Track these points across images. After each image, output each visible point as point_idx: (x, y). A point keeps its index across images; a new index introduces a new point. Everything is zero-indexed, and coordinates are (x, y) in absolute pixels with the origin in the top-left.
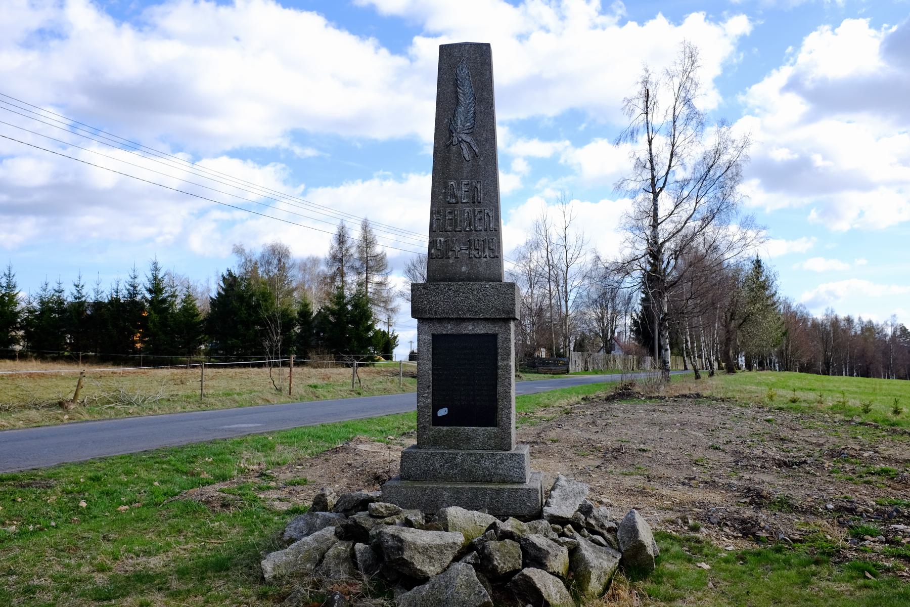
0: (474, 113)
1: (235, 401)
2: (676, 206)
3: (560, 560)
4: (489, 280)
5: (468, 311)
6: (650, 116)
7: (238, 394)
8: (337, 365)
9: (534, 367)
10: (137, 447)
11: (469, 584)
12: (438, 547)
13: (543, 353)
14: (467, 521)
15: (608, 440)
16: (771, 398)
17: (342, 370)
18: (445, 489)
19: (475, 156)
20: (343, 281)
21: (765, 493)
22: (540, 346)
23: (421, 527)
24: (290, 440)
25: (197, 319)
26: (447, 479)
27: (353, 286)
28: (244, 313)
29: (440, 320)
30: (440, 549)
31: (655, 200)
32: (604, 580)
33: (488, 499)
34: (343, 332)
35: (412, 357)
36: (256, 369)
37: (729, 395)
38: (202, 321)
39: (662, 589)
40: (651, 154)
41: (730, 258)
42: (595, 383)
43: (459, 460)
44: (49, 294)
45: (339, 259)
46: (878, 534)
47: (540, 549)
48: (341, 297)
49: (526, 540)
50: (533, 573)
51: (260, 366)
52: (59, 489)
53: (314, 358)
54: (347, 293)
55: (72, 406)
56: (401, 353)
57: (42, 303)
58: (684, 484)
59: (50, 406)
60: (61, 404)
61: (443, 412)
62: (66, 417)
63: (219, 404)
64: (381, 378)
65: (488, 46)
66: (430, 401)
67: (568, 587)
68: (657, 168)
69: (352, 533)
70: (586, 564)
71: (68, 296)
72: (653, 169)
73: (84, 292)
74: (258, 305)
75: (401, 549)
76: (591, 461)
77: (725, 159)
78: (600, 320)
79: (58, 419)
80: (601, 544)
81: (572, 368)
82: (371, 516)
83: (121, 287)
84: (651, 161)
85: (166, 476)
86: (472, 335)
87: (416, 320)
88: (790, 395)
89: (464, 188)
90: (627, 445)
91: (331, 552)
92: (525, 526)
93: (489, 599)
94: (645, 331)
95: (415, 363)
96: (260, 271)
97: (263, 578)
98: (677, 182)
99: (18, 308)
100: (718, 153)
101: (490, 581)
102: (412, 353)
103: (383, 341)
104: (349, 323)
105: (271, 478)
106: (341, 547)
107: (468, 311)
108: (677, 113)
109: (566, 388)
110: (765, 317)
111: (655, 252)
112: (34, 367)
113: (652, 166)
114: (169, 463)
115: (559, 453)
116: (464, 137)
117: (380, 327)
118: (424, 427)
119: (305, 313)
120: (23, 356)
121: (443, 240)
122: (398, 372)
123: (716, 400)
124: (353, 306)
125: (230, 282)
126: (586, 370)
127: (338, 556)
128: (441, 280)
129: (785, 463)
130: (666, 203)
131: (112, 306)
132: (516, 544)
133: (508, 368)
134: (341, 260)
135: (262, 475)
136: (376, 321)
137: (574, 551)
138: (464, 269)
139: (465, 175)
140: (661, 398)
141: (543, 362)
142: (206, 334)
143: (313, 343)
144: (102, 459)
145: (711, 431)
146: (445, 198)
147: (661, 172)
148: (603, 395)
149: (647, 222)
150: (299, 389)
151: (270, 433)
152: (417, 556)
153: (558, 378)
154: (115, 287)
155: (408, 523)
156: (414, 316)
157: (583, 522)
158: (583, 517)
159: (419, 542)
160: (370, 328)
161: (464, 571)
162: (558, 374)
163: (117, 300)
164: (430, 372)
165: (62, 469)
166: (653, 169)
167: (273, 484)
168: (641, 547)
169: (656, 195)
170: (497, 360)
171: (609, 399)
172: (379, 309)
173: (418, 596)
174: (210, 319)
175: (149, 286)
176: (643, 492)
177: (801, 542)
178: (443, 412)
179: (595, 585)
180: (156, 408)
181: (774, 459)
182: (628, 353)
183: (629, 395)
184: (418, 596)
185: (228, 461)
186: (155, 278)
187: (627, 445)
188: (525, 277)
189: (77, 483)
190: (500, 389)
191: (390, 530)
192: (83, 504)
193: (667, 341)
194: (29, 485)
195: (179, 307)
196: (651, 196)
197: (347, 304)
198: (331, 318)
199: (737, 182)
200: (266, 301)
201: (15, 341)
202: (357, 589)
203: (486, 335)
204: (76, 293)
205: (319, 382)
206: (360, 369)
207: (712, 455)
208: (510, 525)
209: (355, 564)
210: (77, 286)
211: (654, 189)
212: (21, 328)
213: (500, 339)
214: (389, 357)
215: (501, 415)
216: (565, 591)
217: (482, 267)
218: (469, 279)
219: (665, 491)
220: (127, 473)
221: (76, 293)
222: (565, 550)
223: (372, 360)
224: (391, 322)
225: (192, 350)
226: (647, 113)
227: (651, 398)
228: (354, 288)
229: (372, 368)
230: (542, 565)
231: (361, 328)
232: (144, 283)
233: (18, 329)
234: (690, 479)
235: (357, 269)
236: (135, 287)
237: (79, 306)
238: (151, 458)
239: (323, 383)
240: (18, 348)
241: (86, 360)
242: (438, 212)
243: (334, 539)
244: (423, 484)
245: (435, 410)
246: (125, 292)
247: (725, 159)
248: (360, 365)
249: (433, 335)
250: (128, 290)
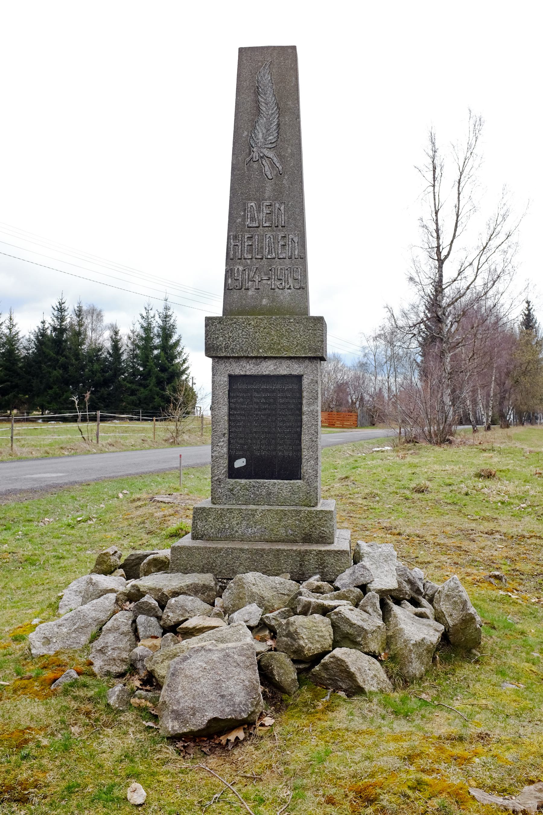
0: (278, 125)
5: (270, 348)
31: (440, 267)
34: (133, 383)
65: (294, 48)
66: (225, 450)
72: (438, 238)
86: (274, 376)
87: (210, 360)
107: (270, 348)
116: (266, 152)
121: (241, 268)
128: (240, 314)
138: (264, 302)
139: (266, 196)
147: (445, 241)
156: (208, 354)
164: (226, 418)
166: (438, 238)
169: (441, 262)
170: (301, 404)
178: (240, 463)
190: (305, 438)
203: (290, 376)
213: (305, 381)
215: (306, 467)
226: (434, 186)
239: (123, 446)
242: (235, 237)
245: (232, 459)
249: (230, 376)
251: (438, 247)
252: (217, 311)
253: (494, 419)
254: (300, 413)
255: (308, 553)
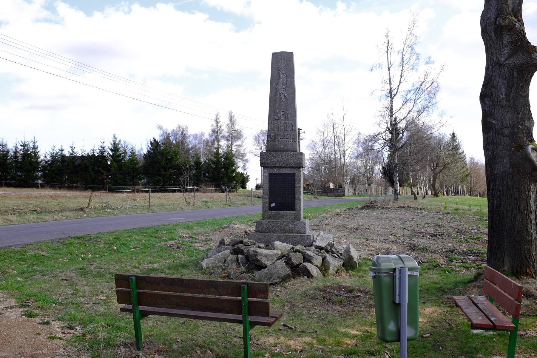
1: (166, 209)
2: (403, 105)
3: (318, 261)
4: (292, 151)
6: (389, 54)
7: (168, 205)
8: (216, 191)
9: (325, 193)
10: (130, 227)
11: (282, 268)
12: (271, 255)
13: (331, 186)
14: (282, 247)
15: (352, 225)
16: (445, 208)
17: (219, 194)
18: (274, 235)
19: (287, 99)
20: (218, 145)
21: (416, 245)
22: (329, 181)
23: (264, 249)
24: (201, 224)
25: (138, 166)
26: (274, 232)
27: (224, 147)
28: (164, 162)
29: (272, 167)
30: (272, 256)
31: (392, 101)
32: (336, 269)
33: (291, 239)
34: (220, 172)
35: (258, 187)
36: (171, 194)
37: (425, 206)
38: (141, 167)
39: (359, 274)
40: (390, 75)
41: (436, 132)
42: (357, 201)
43: (279, 224)
44: (57, 150)
45: (216, 132)
46: (459, 259)
47: (310, 256)
48: (217, 154)
49: (305, 253)
50: (307, 265)
51: (174, 191)
52: (102, 242)
53: (203, 188)
54: (221, 151)
55: (87, 210)
56: (251, 185)
57: (52, 156)
58: (383, 242)
59: (75, 210)
60: (82, 209)
61: (273, 205)
62: (85, 215)
63: (158, 210)
64: (241, 198)
66: (268, 200)
67: (321, 271)
68: (393, 83)
69: (236, 252)
70: (329, 263)
71: (67, 153)
72: (390, 84)
73: (75, 151)
74: (172, 158)
75: (256, 255)
76: (343, 233)
77: (430, 79)
78: (365, 166)
79: (81, 216)
80: (336, 257)
81: (346, 193)
82: (245, 245)
83: (96, 148)
84: (390, 80)
85: (147, 238)
88: (455, 206)
89: (282, 113)
90: (361, 227)
91: (229, 258)
92: (305, 248)
93: (290, 272)
94: (388, 173)
95: (259, 191)
96: (171, 138)
97: (202, 268)
98: (404, 91)
99: (40, 160)
100: (426, 75)
101: (291, 268)
102: (258, 185)
103: (241, 178)
104: (222, 168)
105: (196, 239)
106: (233, 257)
108: (404, 53)
109: (340, 203)
110: (455, 166)
111: (394, 129)
112: (49, 192)
113: (390, 82)
114: (146, 233)
115: (321, 223)
116: (282, 92)
117: (240, 170)
118: (265, 211)
119: (198, 163)
120: (42, 186)
122: (250, 195)
123: (418, 209)
124: (225, 159)
125: (155, 144)
126: (354, 194)
127: (232, 260)
129: (434, 235)
130: (397, 102)
131: (91, 159)
132: (301, 254)
133: (300, 187)
134: (217, 132)
135: (191, 237)
136: (237, 167)
137: (324, 259)
138: (282, 146)
140: (389, 208)
141: (331, 190)
142: (143, 174)
143: (202, 179)
144: (116, 231)
145: (405, 222)
146: (274, 117)
147: (395, 85)
148: (359, 207)
149: (388, 113)
150: (198, 203)
151: (190, 222)
152: (263, 258)
153: (338, 199)
154: (93, 148)
155: (259, 247)
157: (329, 249)
158: (329, 247)
159: (263, 253)
160: (234, 171)
161: (281, 263)
162: (339, 196)
163: (94, 155)
165: (100, 235)
166: (390, 84)
167: (197, 241)
168: (351, 258)
169: (392, 98)
171: (361, 209)
172: (239, 160)
173: (263, 273)
174: (144, 167)
175: (111, 147)
176: (362, 244)
177: (426, 262)
178: (273, 205)
179: (331, 271)
180: (127, 211)
181: (429, 233)
182: (379, 185)
183: (372, 207)
184: (263, 273)
185: (173, 233)
186: (115, 143)
187: (361, 227)
188: (320, 143)
189: (109, 240)
190: (296, 196)
191: (252, 249)
192: (115, 248)
193: (397, 178)
194: (89, 240)
195: (127, 159)
196: (390, 99)
197: (221, 157)
198: (213, 166)
199: (438, 91)
200: (176, 156)
201: (37, 178)
202: (240, 271)
204: (71, 152)
205: (208, 200)
206: (229, 193)
207: (402, 232)
208: (298, 247)
209: (239, 263)
210: (72, 148)
211: (391, 95)
212: (41, 171)
214: (244, 187)
215: (297, 206)
216: (319, 272)
217: (289, 146)
218: (284, 151)
219: (374, 244)
220: (130, 237)
221: (71, 152)
222: (320, 258)
223: (235, 189)
224: (246, 168)
225: (135, 184)
226: (388, 53)
227: (384, 208)
228: (225, 149)
229: (235, 193)
230: (310, 262)
231: (229, 171)
232: (108, 146)
233: (39, 171)
234: (386, 240)
235: (226, 137)
236: (103, 148)
237: (73, 158)
238: (140, 231)
239: (208, 201)
240: (40, 182)
241: (77, 188)
242: (271, 123)
243: (229, 254)
244: (265, 233)
245: (270, 204)
246: (98, 151)
247: (430, 79)
248: (230, 191)
250: (100, 149)
251: (390, 89)
252: (264, 149)
253: (306, 178)
254: (295, 187)
255: (295, 236)
